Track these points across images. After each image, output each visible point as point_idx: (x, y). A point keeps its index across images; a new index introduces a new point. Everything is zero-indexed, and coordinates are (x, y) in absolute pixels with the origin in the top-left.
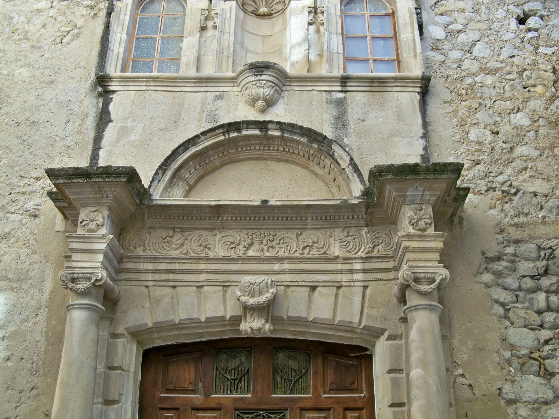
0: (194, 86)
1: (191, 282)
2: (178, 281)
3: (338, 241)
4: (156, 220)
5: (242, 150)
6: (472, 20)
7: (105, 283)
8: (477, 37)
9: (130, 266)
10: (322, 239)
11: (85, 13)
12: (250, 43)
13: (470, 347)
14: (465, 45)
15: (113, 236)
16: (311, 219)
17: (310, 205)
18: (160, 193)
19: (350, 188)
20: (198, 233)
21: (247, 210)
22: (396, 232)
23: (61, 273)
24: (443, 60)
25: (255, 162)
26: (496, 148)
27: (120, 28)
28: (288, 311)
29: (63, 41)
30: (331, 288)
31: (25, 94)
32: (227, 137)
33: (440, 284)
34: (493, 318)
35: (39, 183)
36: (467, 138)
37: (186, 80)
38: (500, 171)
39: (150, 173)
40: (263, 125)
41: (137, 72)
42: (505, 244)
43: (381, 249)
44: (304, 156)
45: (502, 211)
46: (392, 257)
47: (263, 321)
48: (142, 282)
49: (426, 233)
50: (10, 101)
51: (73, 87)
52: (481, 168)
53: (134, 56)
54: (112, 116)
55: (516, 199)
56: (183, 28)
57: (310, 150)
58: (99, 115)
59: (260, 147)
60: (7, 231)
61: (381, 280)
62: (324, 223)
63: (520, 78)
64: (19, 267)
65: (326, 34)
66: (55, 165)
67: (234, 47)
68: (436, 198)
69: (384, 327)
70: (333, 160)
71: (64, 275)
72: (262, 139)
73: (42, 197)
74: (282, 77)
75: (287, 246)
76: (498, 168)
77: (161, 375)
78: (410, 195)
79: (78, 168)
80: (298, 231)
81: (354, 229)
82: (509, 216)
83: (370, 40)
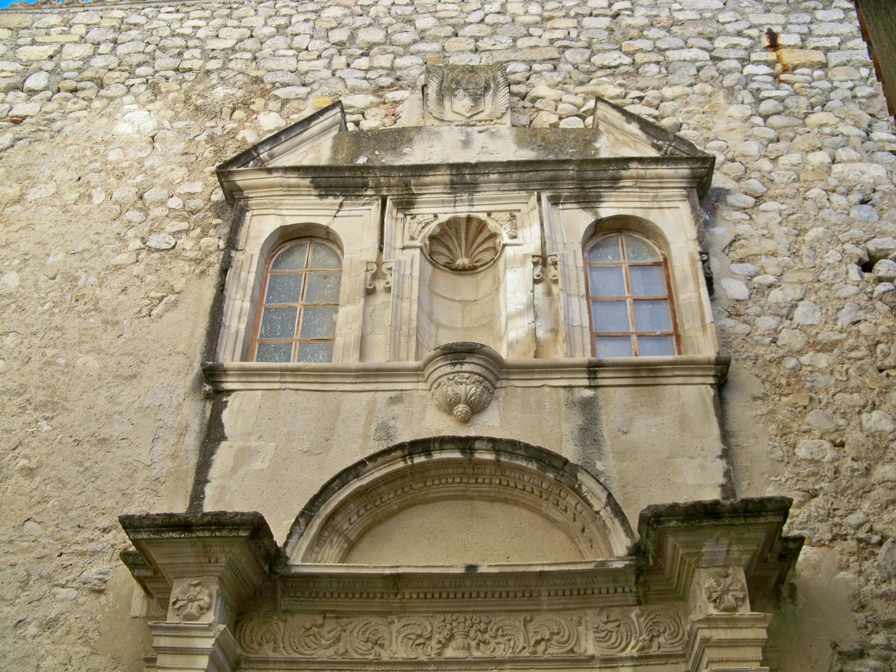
0: (356, 383)
3: (592, 631)
6: (789, 268)
8: (798, 294)
11: (187, 269)
12: (445, 313)
14: (780, 307)
18: (301, 556)
22: (687, 613)
24: (748, 332)
25: (454, 503)
26: (842, 469)
27: (241, 293)
29: (153, 312)
31: (91, 395)
32: (409, 463)
35: (108, 536)
36: (794, 454)
37: (343, 373)
38: (851, 507)
39: (286, 523)
40: (466, 444)
41: (266, 361)
42: (870, 629)
44: (533, 492)
45: (860, 573)
46: (683, 656)
49: (737, 614)
50: (68, 406)
51: (165, 385)
52: (820, 502)
53: (261, 336)
54: (226, 431)
55: (882, 551)
56: (338, 292)
58: (205, 429)
60: (53, 615)
63: (872, 356)
65: (562, 296)
66: (134, 510)
67: (418, 320)
68: (749, 556)
73: (111, 560)
74: (494, 366)
75: (510, 640)
76: (848, 502)
78: (706, 552)
79: (171, 516)
80: (526, 614)
81: (617, 610)
82: (872, 582)
83: (631, 304)
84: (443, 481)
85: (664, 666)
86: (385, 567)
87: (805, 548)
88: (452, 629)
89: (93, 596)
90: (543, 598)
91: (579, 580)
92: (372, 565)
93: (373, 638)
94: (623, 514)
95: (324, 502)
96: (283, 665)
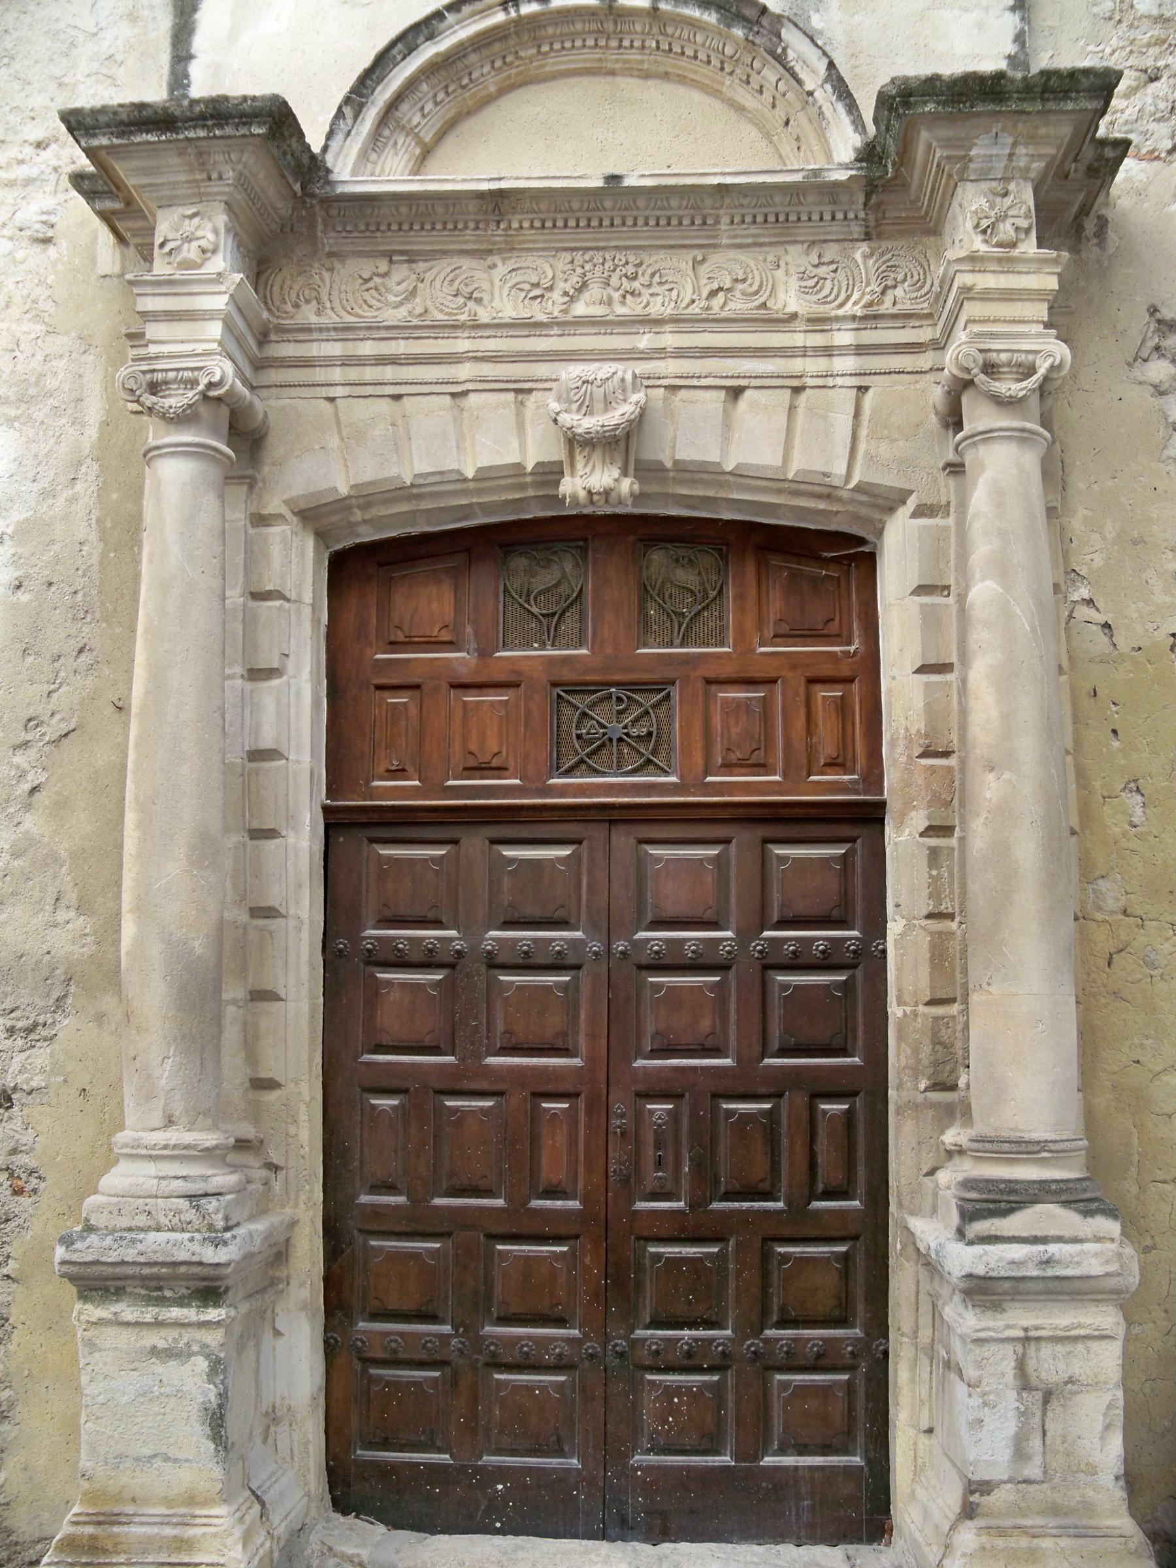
1: (436, 383)
2: (406, 383)
3: (795, 277)
4: (344, 234)
5: (552, 49)
7: (231, 392)
9: (287, 350)
10: (756, 272)
13: (1110, 537)
15: (241, 275)
16: (728, 221)
17: (726, 185)
19: (827, 141)
20: (449, 265)
21: (569, 202)
22: (939, 255)
23: (123, 372)
25: (584, 81)
28: (674, 448)
30: (778, 391)
32: (513, 14)
33: (1046, 379)
34: (1168, 468)
35: (47, 155)
39: (321, 118)
43: (902, 298)
44: (709, 62)
47: (616, 473)
48: (318, 388)
49: (1016, 252)
57: (724, 45)
59: (596, 40)
61: (899, 372)
62: (760, 231)
64: (20, 368)
68: (1043, 164)
69: (907, 486)
70: (782, 71)
71: (132, 376)
72: (603, 18)
73: (55, 192)
75: (671, 290)
77: (373, 611)
78: (978, 156)
79: (142, 106)
84: (568, 45)
85: (901, 331)
86: (479, 180)
87: (1128, 163)
88: (584, 274)
89: (38, 248)
90: (723, 227)
91: (778, 199)
92: (460, 177)
93: (466, 290)
94: (850, 95)
95: (380, 80)
96: (332, 333)
